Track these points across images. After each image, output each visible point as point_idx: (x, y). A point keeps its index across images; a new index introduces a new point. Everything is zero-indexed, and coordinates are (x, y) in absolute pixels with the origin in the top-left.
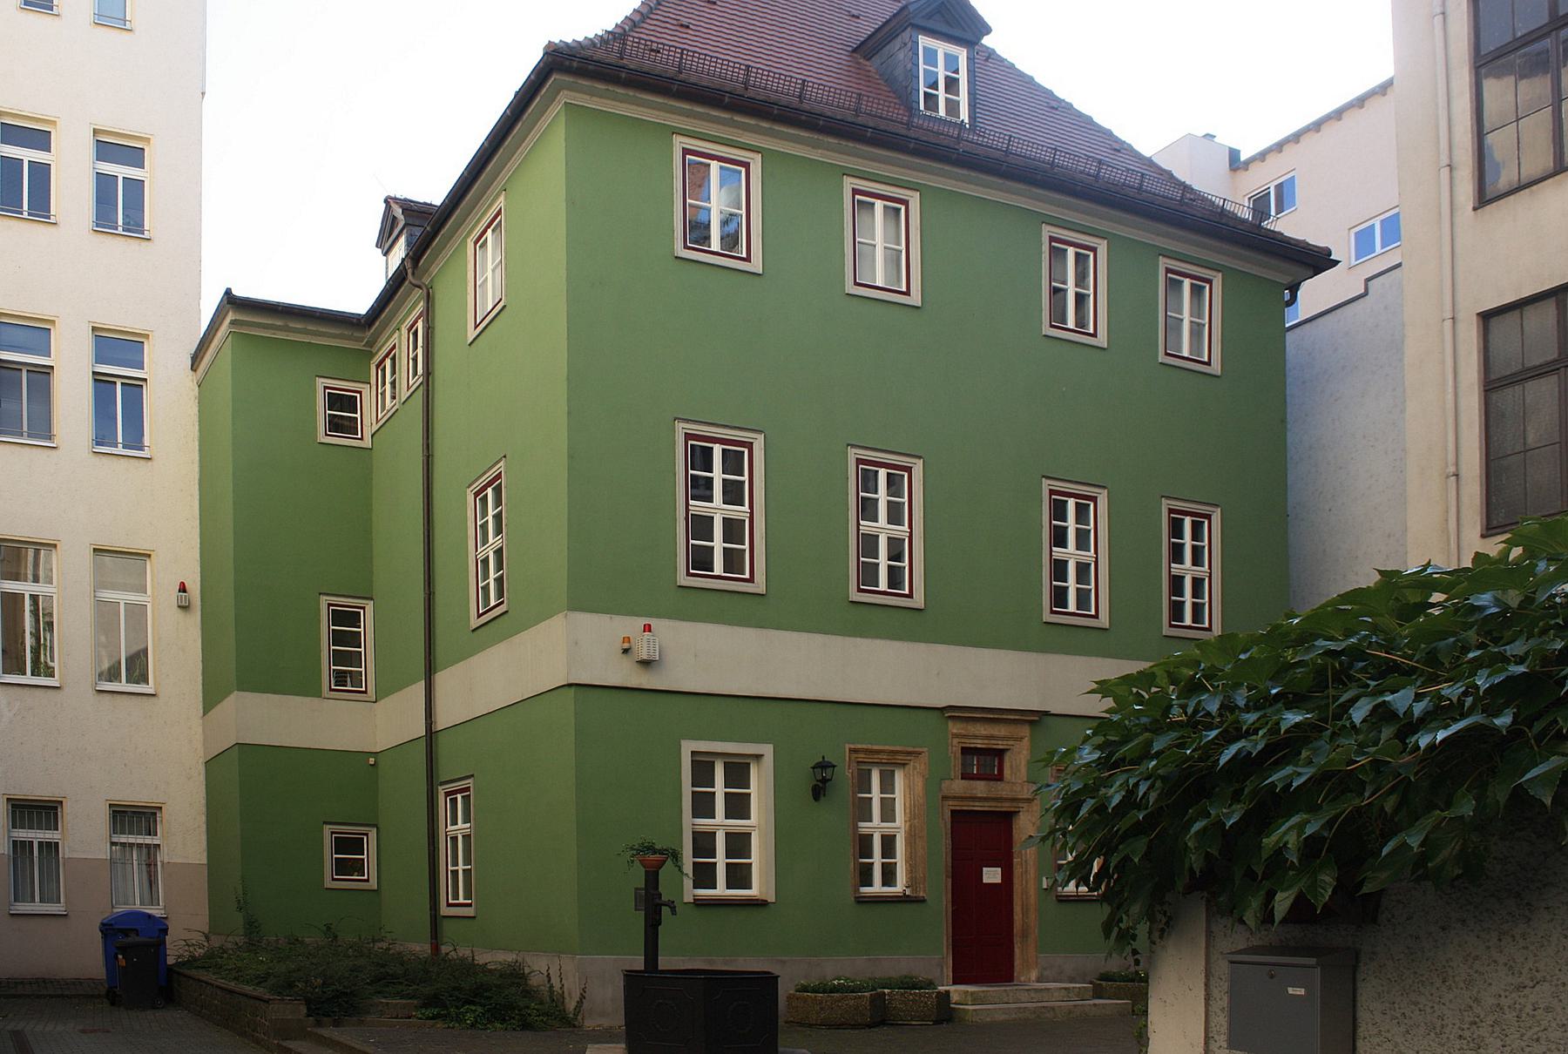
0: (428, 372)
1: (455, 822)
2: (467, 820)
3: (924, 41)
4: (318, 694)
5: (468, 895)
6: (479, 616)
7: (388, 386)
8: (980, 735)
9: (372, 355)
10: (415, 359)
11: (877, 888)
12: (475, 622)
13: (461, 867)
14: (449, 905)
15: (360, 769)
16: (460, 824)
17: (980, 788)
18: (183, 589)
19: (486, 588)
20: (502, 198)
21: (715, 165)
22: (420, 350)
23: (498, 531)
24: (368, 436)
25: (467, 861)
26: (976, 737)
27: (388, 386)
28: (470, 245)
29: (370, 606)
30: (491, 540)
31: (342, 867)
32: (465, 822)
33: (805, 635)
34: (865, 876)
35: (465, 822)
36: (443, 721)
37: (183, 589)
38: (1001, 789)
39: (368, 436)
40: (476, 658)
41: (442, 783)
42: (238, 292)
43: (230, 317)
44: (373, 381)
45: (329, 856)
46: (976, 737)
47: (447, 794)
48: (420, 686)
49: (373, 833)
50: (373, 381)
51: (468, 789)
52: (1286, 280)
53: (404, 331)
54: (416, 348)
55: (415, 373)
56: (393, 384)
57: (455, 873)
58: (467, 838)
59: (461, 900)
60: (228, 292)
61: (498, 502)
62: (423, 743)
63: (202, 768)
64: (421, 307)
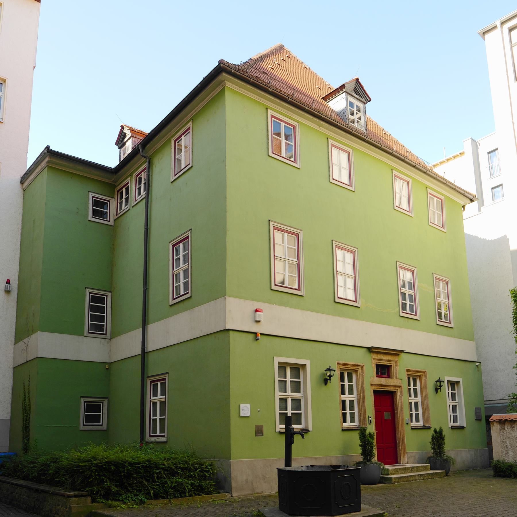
1: (155, 395)
2: (163, 393)
4: (82, 335)
5: (162, 430)
6: (174, 299)
7: (124, 200)
9: (115, 186)
12: (172, 302)
13: (158, 417)
14: (150, 436)
15: (107, 370)
16: (159, 396)
17: (383, 381)
18: (8, 282)
24: (112, 220)
26: (380, 360)
27: (124, 200)
28: (173, 142)
29: (110, 295)
30: (182, 265)
31: (89, 419)
32: (161, 395)
35: (161, 395)
36: (151, 346)
37: (8, 282)
39: (112, 220)
40: (172, 318)
41: (148, 377)
42: (52, 148)
43: (47, 159)
45: (83, 413)
47: (151, 382)
48: (140, 330)
49: (106, 402)
52: (463, 203)
53: (134, 176)
56: (127, 199)
57: (155, 421)
58: (163, 403)
59: (158, 433)
60: (48, 147)
62: (140, 358)
63: (12, 371)
64: (146, 165)
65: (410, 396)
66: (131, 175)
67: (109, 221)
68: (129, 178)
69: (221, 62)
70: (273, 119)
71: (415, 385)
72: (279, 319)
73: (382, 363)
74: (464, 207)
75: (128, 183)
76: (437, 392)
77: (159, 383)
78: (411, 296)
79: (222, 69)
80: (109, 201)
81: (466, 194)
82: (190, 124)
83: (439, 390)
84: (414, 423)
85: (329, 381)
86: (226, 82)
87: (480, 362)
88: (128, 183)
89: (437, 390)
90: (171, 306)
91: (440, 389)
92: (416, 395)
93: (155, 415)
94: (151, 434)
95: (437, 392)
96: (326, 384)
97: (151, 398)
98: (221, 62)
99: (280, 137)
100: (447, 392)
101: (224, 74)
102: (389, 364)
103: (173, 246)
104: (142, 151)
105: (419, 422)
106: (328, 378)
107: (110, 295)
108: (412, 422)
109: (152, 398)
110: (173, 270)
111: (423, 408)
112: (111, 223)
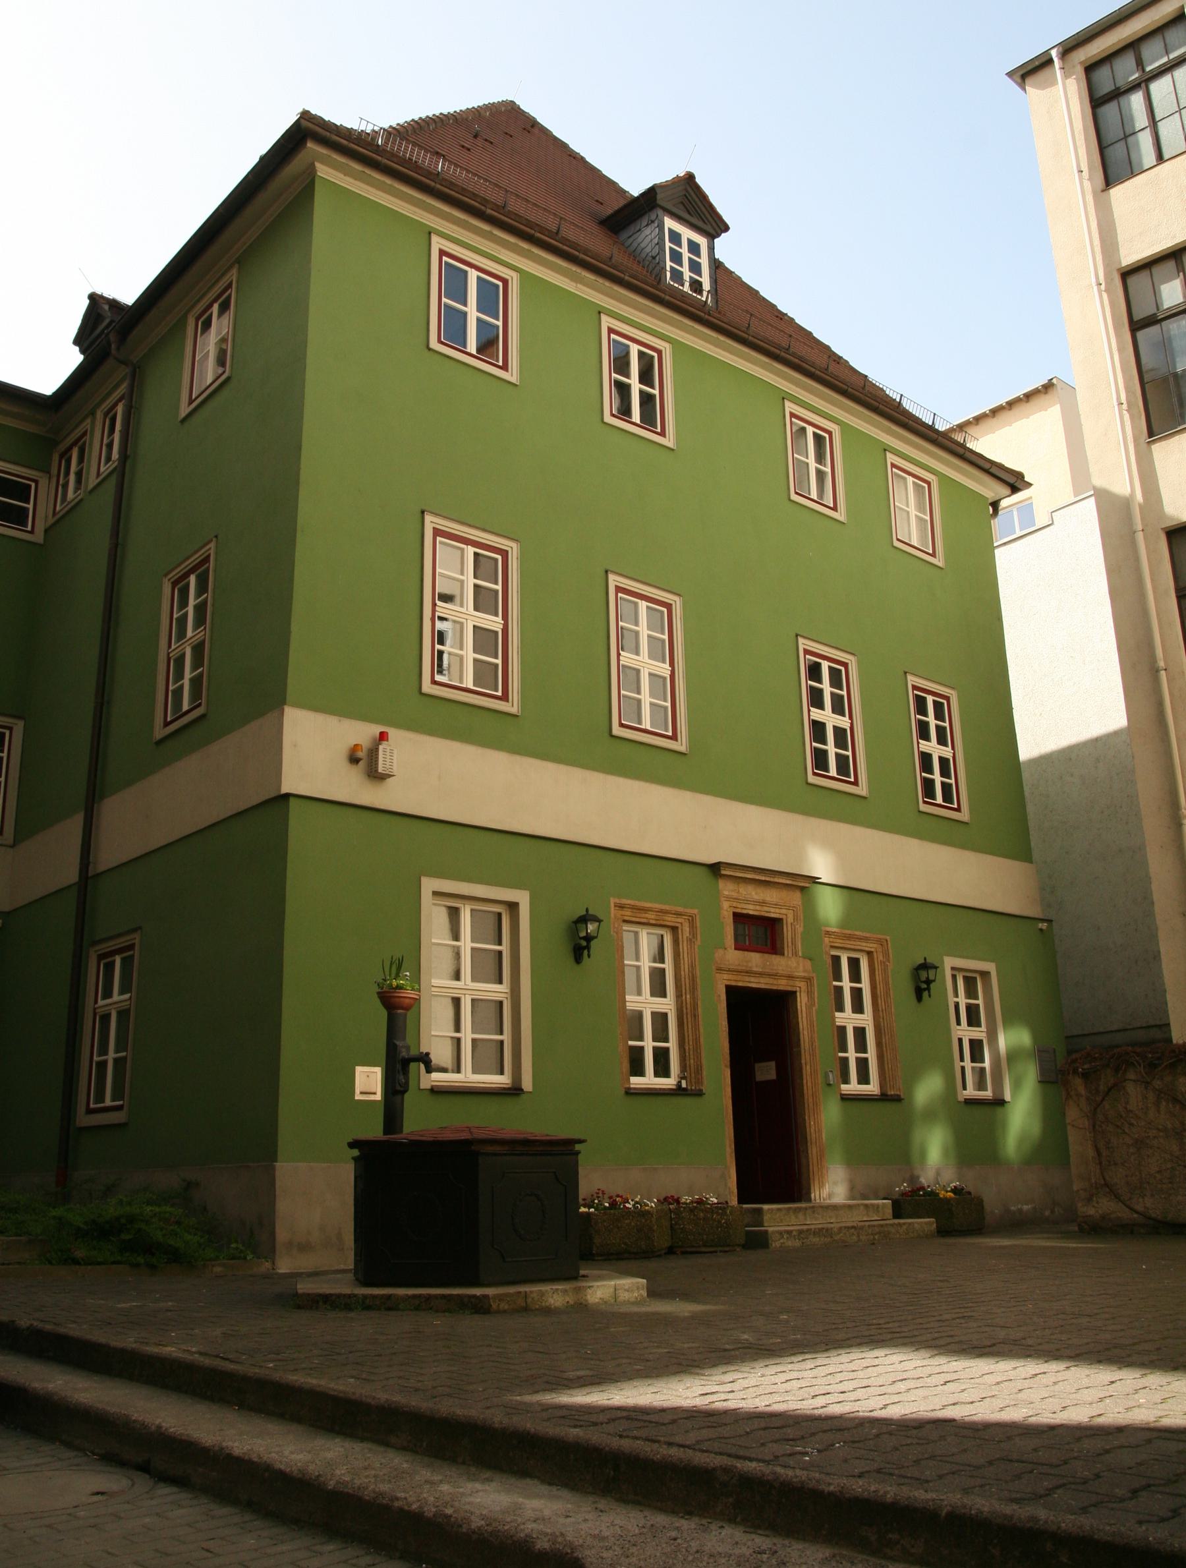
0: (124, 456)
1: (108, 994)
3: (669, 223)
5: (118, 1094)
6: (167, 724)
7: (72, 478)
8: (756, 901)
10: (110, 446)
11: (649, 1080)
12: (159, 732)
14: (90, 1111)
16: (116, 997)
17: (755, 960)
19: (178, 692)
20: (234, 271)
21: (643, 605)
22: (117, 437)
23: (200, 620)
25: (121, 1045)
26: (747, 901)
27: (72, 478)
30: (190, 633)
33: (562, 767)
34: (638, 1070)
35: (121, 993)
38: (778, 963)
44: (54, 471)
46: (747, 901)
47: (101, 957)
48: (78, 819)
49: (19, 727)
50: (54, 471)
51: (131, 947)
53: (99, 415)
54: (112, 430)
55: (109, 459)
56: (79, 474)
57: (102, 1065)
58: (123, 1014)
59: (108, 1102)
61: (202, 588)
65: (841, 1008)
66: (93, 413)
67: (32, 532)
68: (89, 420)
69: (305, 115)
70: (613, 336)
71: (855, 976)
72: (436, 777)
73: (751, 910)
74: (995, 505)
75: (85, 434)
76: (919, 998)
77: (118, 960)
78: (839, 733)
79: (306, 133)
80: (36, 482)
81: (994, 470)
82: (233, 275)
83: (925, 994)
84: (853, 1086)
85: (586, 952)
86: (318, 165)
87: (1049, 921)
88: (85, 434)
89: (919, 993)
90: (160, 742)
91: (928, 989)
92: (858, 1008)
93: (104, 1050)
94: (92, 1106)
95: (919, 998)
96: (578, 959)
97: (96, 1002)
98: (305, 115)
99: (465, 305)
100: (952, 1000)
101: (310, 145)
102: (774, 913)
103: (174, 584)
104: (118, 349)
105: (867, 1082)
106: (584, 943)
107: (19, 727)
108: (846, 1081)
109: (101, 1002)
110: (170, 646)
111: (879, 1044)
112: (39, 537)
